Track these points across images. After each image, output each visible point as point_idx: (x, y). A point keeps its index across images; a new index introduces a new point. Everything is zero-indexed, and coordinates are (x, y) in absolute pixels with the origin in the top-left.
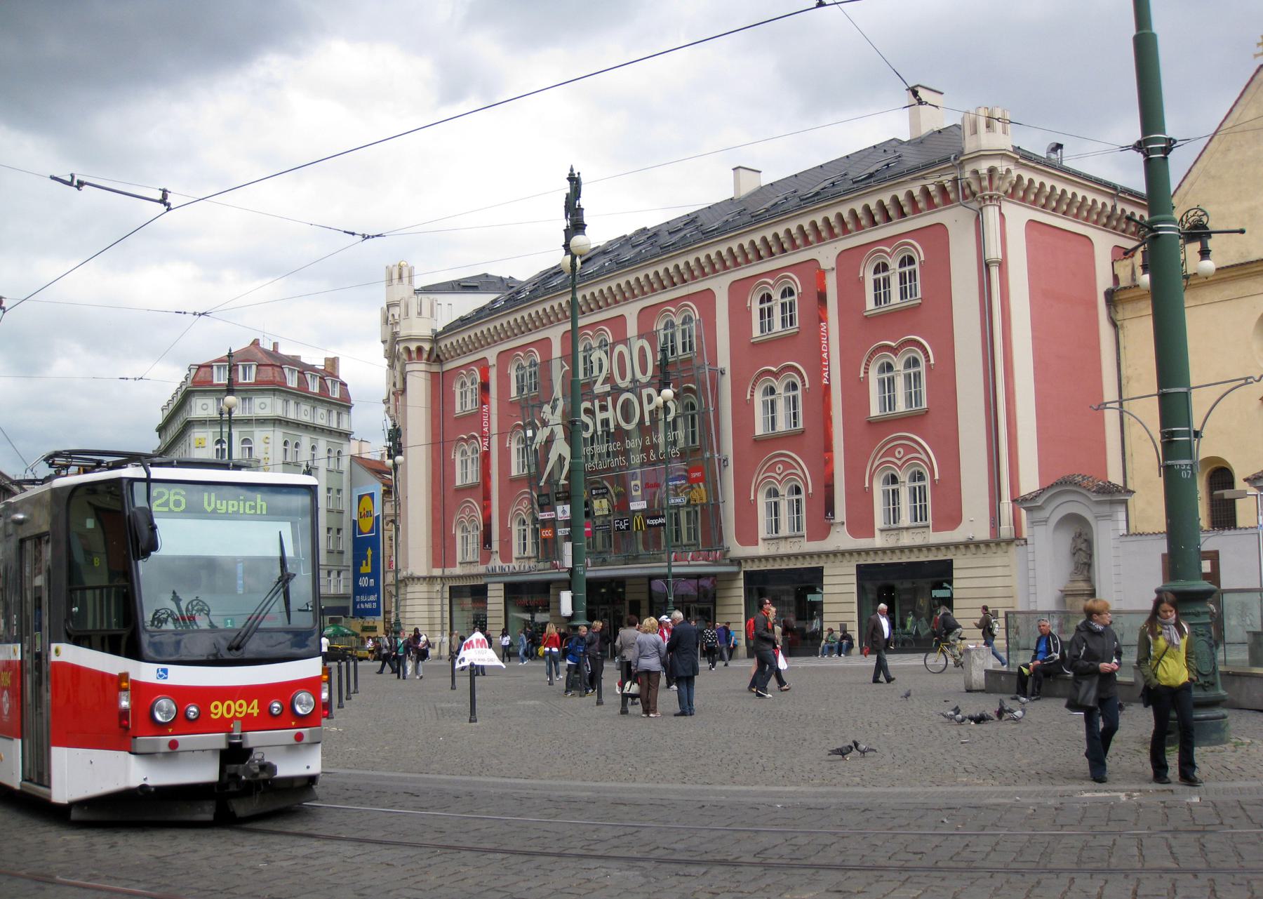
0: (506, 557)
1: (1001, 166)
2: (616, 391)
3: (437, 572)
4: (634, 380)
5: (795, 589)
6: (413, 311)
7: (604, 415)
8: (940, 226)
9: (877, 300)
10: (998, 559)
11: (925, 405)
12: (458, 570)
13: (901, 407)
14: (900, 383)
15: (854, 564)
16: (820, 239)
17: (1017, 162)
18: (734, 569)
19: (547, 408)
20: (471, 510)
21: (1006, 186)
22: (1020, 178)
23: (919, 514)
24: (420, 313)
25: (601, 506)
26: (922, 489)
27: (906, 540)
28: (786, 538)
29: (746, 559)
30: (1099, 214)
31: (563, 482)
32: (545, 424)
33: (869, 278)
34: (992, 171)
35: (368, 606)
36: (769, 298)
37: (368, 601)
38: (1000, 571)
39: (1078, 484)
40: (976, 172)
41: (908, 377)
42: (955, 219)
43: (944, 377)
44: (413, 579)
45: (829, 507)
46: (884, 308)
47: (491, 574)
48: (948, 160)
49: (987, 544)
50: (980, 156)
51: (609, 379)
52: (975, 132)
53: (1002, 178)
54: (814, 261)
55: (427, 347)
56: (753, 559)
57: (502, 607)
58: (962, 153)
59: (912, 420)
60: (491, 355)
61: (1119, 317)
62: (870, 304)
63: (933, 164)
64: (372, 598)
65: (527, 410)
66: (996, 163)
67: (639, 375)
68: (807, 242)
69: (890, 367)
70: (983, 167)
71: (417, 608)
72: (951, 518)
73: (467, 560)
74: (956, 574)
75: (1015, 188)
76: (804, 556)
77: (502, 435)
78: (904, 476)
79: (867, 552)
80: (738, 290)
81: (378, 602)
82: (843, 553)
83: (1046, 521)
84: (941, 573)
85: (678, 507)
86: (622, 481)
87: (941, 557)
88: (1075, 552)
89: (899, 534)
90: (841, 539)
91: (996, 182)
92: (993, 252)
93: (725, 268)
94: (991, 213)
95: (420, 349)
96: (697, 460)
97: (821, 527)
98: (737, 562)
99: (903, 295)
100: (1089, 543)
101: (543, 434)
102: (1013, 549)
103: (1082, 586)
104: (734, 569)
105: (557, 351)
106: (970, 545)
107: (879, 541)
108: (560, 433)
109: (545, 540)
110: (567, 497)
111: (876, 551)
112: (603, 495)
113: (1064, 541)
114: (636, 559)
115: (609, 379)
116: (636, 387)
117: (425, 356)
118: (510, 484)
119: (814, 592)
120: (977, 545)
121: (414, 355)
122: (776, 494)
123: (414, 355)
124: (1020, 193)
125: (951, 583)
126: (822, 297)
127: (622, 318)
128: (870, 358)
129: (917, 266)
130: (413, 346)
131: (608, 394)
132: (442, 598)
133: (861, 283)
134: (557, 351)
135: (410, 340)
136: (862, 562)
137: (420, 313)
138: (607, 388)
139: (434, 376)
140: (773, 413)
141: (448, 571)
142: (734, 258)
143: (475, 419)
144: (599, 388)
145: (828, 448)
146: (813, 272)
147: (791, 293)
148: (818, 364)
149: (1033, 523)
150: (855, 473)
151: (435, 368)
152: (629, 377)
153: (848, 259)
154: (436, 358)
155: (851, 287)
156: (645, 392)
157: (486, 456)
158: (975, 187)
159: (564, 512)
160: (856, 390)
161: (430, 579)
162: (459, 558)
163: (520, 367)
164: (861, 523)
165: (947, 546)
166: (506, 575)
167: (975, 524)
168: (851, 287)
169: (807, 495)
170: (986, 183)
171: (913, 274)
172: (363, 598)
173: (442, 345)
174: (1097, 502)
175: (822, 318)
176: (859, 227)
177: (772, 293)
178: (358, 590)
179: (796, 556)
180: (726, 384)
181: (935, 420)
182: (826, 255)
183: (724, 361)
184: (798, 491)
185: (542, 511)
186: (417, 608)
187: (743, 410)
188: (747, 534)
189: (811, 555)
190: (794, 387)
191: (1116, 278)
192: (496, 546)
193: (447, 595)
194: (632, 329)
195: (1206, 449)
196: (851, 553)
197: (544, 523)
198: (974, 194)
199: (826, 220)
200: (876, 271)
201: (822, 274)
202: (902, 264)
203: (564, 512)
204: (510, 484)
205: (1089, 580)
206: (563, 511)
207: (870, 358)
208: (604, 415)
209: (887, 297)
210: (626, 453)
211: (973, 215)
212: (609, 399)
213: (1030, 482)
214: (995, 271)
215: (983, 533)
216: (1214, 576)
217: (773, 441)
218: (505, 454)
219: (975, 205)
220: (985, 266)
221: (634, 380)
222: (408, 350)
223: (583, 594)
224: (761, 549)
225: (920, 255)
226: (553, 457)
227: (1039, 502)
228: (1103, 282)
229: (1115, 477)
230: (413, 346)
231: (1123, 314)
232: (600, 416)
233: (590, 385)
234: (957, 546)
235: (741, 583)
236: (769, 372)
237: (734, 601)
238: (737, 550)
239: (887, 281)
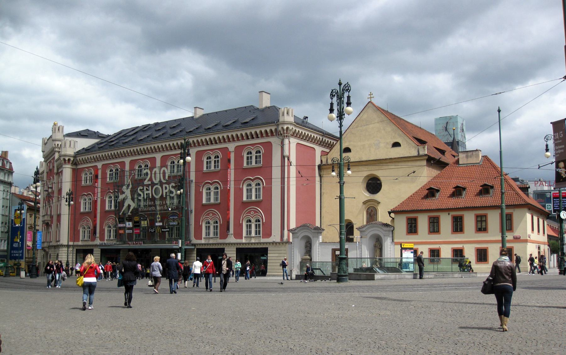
0: (102, 238)
1: (290, 127)
2: (153, 184)
3: (71, 243)
4: (160, 181)
5: (217, 254)
6: (68, 145)
7: (147, 192)
8: (270, 143)
9: (207, 168)
10: (282, 248)
11: (261, 198)
12: (80, 243)
13: (212, 201)
14: (212, 194)
15: (235, 247)
16: (229, 141)
17: (295, 125)
18: (193, 247)
19: (125, 187)
20: (87, 221)
21: (291, 133)
22: (295, 130)
23: (215, 234)
24: (70, 146)
25: (144, 224)
26: (217, 226)
27: (211, 241)
28: (212, 238)
29: (197, 244)
30: (326, 144)
31: (129, 214)
32: (123, 193)
33: (205, 161)
34: (287, 128)
35: (17, 255)
36: (210, 158)
37: (16, 253)
38: (283, 252)
39: (308, 227)
40: (283, 128)
41: (256, 189)
42: (275, 141)
43: (268, 191)
44: (62, 246)
45: (228, 229)
46: (250, 166)
47: (96, 246)
48: (274, 122)
49: (279, 243)
50: (284, 123)
51: (151, 179)
52: (283, 115)
53: (291, 130)
54: (96, 166)
55: (72, 159)
56: (200, 244)
57: (99, 257)
58: (279, 120)
59: (257, 203)
60: (99, 165)
61: (322, 173)
62: (205, 169)
63: (269, 123)
64: (21, 252)
65: (118, 187)
66: (289, 126)
67: (162, 180)
68: (225, 141)
69: (210, 189)
70: (285, 127)
71: (63, 257)
72: (268, 234)
73: (83, 241)
74: (269, 252)
75: (294, 133)
76: (218, 244)
77: (102, 195)
78: (253, 220)
79: (240, 244)
80: (132, 163)
81: (22, 253)
82: (232, 244)
83: (298, 237)
84: (264, 251)
85: (174, 225)
86: (154, 215)
87: (221, 247)
88: (306, 247)
89: (250, 238)
90: (231, 239)
91: (288, 132)
92: (286, 153)
93: (160, 151)
94: (286, 141)
95: (69, 160)
96: (181, 210)
97: (225, 235)
98: (194, 245)
99: (256, 162)
100: (311, 244)
101: (124, 196)
102: (287, 245)
103: (308, 257)
104: (193, 247)
105: (127, 168)
106: (273, 243)
107: (244, 241)
108: (130, 197)
109: (120, 234)
110: (130, 219)
111: (202, 244)
112: (145, 220)
113: (303, 243)
114: (156, 242)
115: (151, 179)
116: (161, 183)
117: (71, 162)
118: (105, 214)
119: (263, 256)
120: (276, 243)
121: (67, 162)
122: (209, 223)
123: (67, 162)
124: (296, 135)
125: (267, 255)
126: (229, 161)
127: (124, 162)
128: (243, 183)
129: (219, 159)
130: (67, 159)
131: (149, 185)
132: (73, 253)
133: (242, 157)
134: (127, 168)
135: (66, 156)
136: (238, 247)
137: (70, 146)
138: (150, 183)
139: (74, 170)
140: (209, 196)
141: (76, 243)
142: (159, 149)
143: (92, 189)
144: (146, 182)
145: (228, 209)
146: (225, 151)
147: (218, 157)
148: (225, 181)
149: (293, 238)
150: (237, 218)
151: (74, 167)
152: (158, 180)
153: (239, 149)
154: (75, 163)
155: (239, 158)
156: (164, 186)
157: (96, 202)
158: (282, 132)
159: (129, 224)
160: (239, 192)
161: (68, 246)
162: (81, 239)
163: (111, 171)
164: (238, 235)
165: (267, 243)
166: (106, 246)
167: (275, 237)
168: (239, 158)
169: (220, 224)
170: (285, 132)
171: (218, 161)
172: (15, 252)
173: (78, 159)
174: (314, 233)
175: (228, 167)
176: (203, 145)
177: (211, 156)
178: (13, 248)
179: (215, 244)
180: (193, 186)
181: (264, 203)
182: (231, 146)
183: (193, 176)
184: (217, 222)
185: (120, 223)
186: (63, 257)
187: (199, 195)
188: (198, 235)
189: (221, 244)
190: (217, 188)
191: (321, 161)
192: (98, 235)
193: (75, 252)
194: (158, 163)
195: (346, 217)
196: (234, 244)
197: (121, 228)
198: (281, 134)
199: (202, 140)
200: (207, 159)
201: (98, 170)
202: (256, 153)
203: (129, 224)
204: (105, 214)
205: (310, 255)
206: (129, 224)
207: (243, 183)
208: (147, 192)
209: (210, 167)
210: (155, 206)
211: (280, 141)
212: (150, 187)
213: (293, 225)
214: (286, 159)
215: (278, 239)
216: (347, 255)
217: (110, 212)
218: (103, 202)
219: (281, 138)
220: (283, 157)
221: (160, 181)
222: (65, 160)
223: (183, 254)
224: (203, 241)
225: (263, 151)
226: (126, 205)
227: (296, 231)
228: (318, 162)
229: (318, 224)
230: (67, 159)
231: (324, 173)
232: (145, 193)
233: (143, 180)
234: (270, 243)
235: (195, 252)
236: (85, 195)
237: (192, 258)
238: (195, 241)
239: (251, 157)
